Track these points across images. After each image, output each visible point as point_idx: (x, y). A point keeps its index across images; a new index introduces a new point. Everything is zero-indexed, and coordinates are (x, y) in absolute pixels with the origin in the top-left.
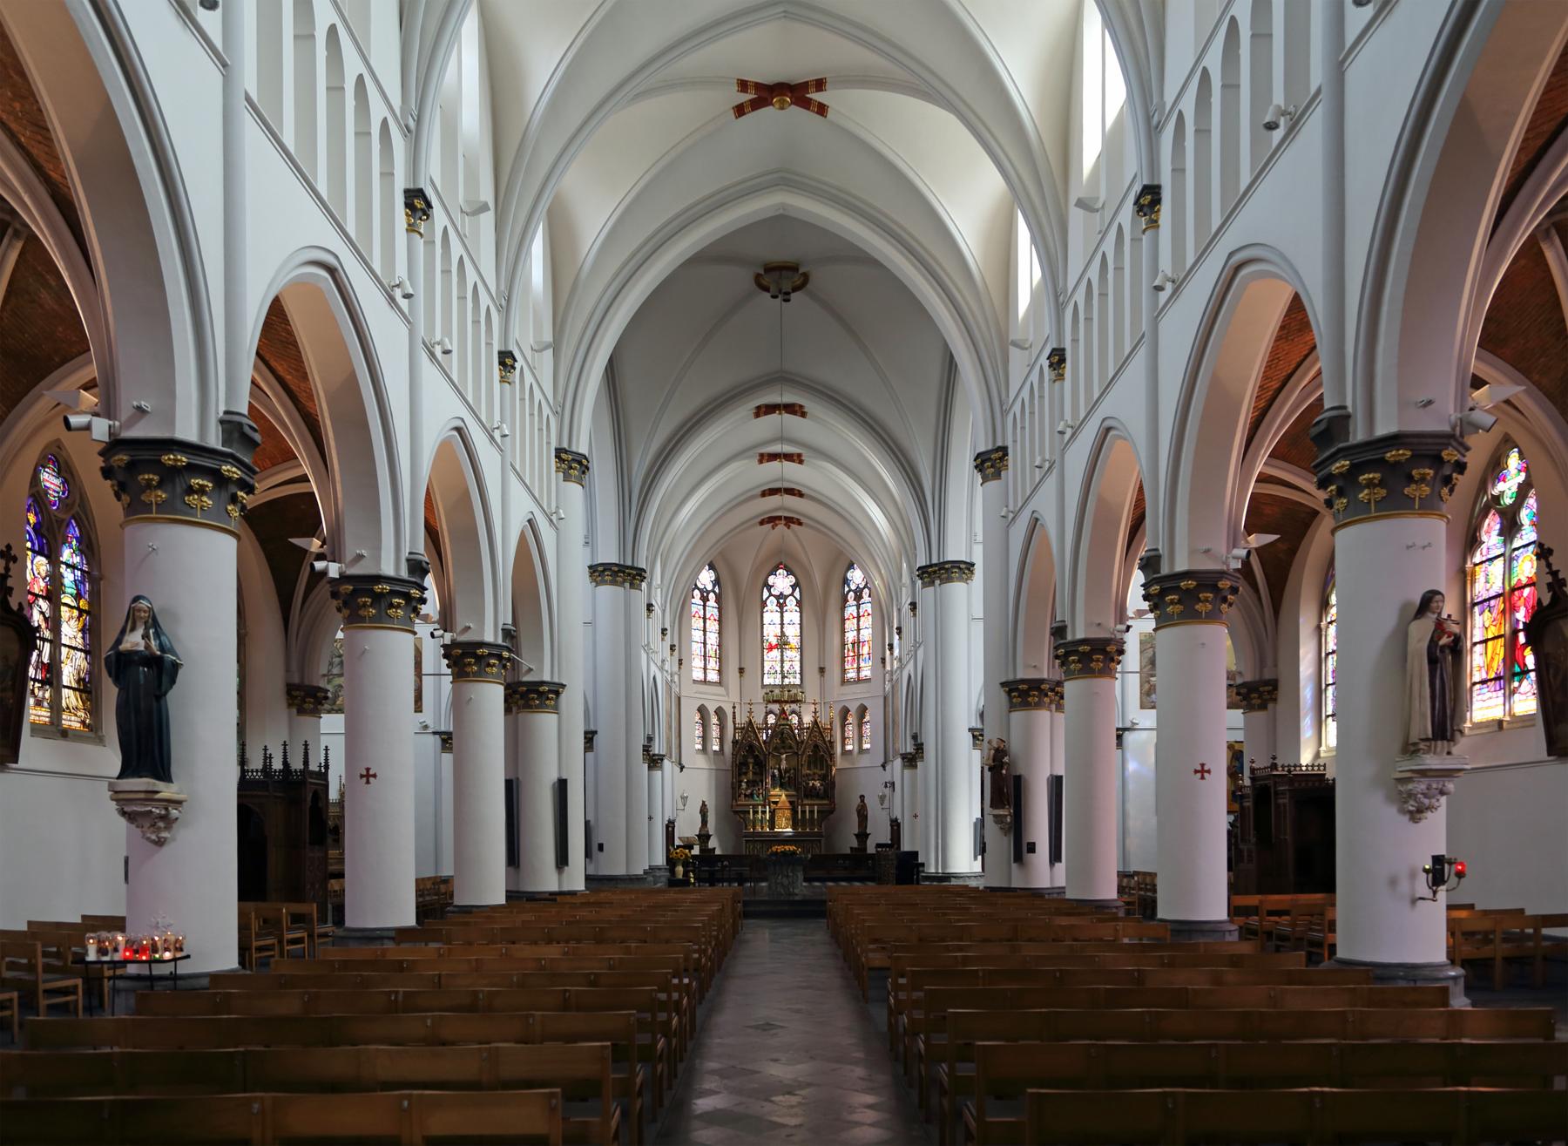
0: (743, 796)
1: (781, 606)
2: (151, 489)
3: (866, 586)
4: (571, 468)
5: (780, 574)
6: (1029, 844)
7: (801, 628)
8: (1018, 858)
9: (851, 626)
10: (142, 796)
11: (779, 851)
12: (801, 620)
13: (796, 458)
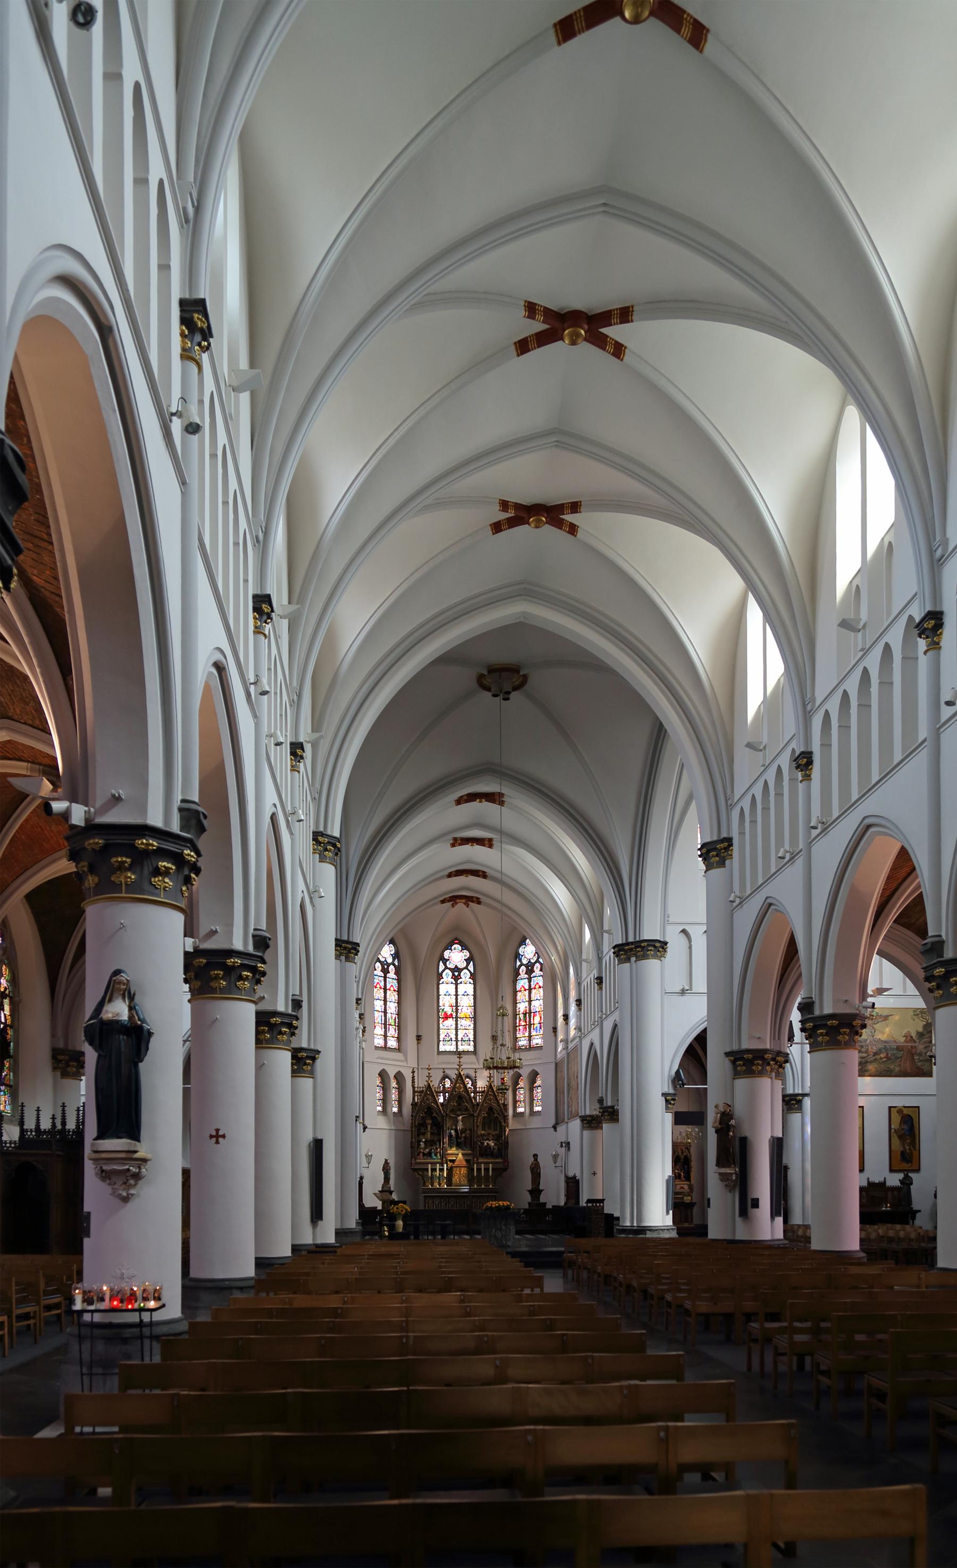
0: (421, 1155)
1: (456, 978)
2: (121, 871)
3: (537, 961)
4: (326, 850)
5: (455, 949)
6: (753, 1200)
7: (475, 999)
8: (744, 1213)
9: (523, 997)
10: (123, 1155)
11: (494, 1206)
12: (475, 991)
13: (487, 843)
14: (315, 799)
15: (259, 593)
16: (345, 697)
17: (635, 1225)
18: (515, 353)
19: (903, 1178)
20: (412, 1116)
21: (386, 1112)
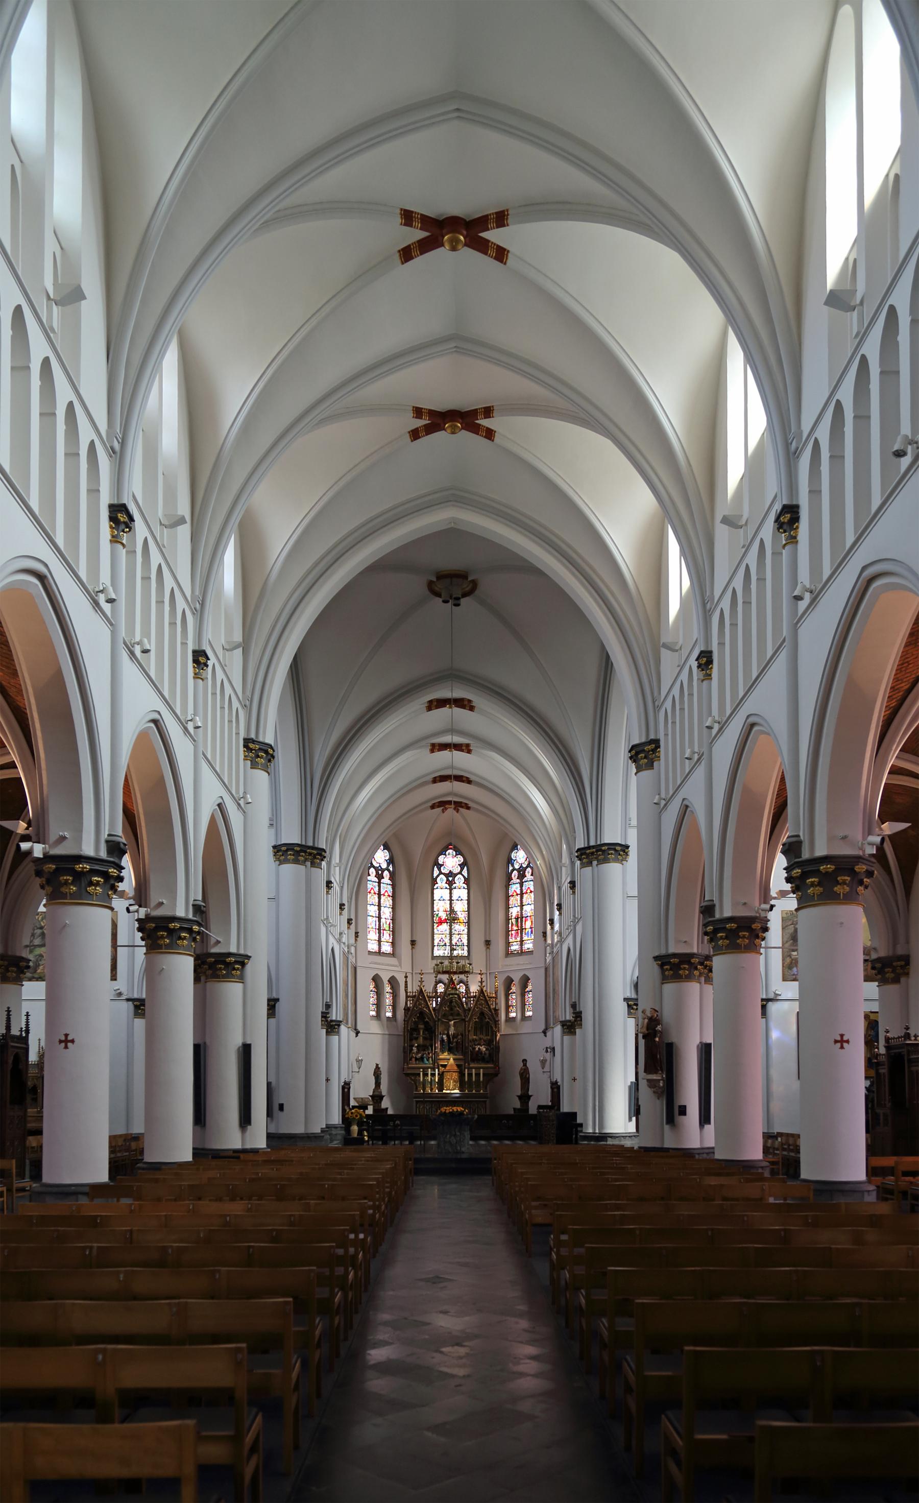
0: (414, 1059)
1: (450, 884)
3: (528, 866)
4: (258, 756)
5: (449, 854)
6: (680, 1107)
7: (469, 904)
9: (515, 902)
11: (447, 1111)
12: (469, 896)
14: (245, 706)
15: (116, 502)
16: (276, 605)
17: (597, 1131)
18: (399, 261)
19: (870, 1086)
20: (404, 1020)
21: (380, 1017)
